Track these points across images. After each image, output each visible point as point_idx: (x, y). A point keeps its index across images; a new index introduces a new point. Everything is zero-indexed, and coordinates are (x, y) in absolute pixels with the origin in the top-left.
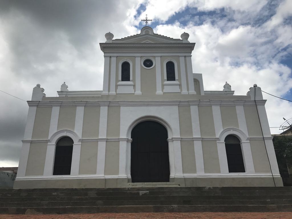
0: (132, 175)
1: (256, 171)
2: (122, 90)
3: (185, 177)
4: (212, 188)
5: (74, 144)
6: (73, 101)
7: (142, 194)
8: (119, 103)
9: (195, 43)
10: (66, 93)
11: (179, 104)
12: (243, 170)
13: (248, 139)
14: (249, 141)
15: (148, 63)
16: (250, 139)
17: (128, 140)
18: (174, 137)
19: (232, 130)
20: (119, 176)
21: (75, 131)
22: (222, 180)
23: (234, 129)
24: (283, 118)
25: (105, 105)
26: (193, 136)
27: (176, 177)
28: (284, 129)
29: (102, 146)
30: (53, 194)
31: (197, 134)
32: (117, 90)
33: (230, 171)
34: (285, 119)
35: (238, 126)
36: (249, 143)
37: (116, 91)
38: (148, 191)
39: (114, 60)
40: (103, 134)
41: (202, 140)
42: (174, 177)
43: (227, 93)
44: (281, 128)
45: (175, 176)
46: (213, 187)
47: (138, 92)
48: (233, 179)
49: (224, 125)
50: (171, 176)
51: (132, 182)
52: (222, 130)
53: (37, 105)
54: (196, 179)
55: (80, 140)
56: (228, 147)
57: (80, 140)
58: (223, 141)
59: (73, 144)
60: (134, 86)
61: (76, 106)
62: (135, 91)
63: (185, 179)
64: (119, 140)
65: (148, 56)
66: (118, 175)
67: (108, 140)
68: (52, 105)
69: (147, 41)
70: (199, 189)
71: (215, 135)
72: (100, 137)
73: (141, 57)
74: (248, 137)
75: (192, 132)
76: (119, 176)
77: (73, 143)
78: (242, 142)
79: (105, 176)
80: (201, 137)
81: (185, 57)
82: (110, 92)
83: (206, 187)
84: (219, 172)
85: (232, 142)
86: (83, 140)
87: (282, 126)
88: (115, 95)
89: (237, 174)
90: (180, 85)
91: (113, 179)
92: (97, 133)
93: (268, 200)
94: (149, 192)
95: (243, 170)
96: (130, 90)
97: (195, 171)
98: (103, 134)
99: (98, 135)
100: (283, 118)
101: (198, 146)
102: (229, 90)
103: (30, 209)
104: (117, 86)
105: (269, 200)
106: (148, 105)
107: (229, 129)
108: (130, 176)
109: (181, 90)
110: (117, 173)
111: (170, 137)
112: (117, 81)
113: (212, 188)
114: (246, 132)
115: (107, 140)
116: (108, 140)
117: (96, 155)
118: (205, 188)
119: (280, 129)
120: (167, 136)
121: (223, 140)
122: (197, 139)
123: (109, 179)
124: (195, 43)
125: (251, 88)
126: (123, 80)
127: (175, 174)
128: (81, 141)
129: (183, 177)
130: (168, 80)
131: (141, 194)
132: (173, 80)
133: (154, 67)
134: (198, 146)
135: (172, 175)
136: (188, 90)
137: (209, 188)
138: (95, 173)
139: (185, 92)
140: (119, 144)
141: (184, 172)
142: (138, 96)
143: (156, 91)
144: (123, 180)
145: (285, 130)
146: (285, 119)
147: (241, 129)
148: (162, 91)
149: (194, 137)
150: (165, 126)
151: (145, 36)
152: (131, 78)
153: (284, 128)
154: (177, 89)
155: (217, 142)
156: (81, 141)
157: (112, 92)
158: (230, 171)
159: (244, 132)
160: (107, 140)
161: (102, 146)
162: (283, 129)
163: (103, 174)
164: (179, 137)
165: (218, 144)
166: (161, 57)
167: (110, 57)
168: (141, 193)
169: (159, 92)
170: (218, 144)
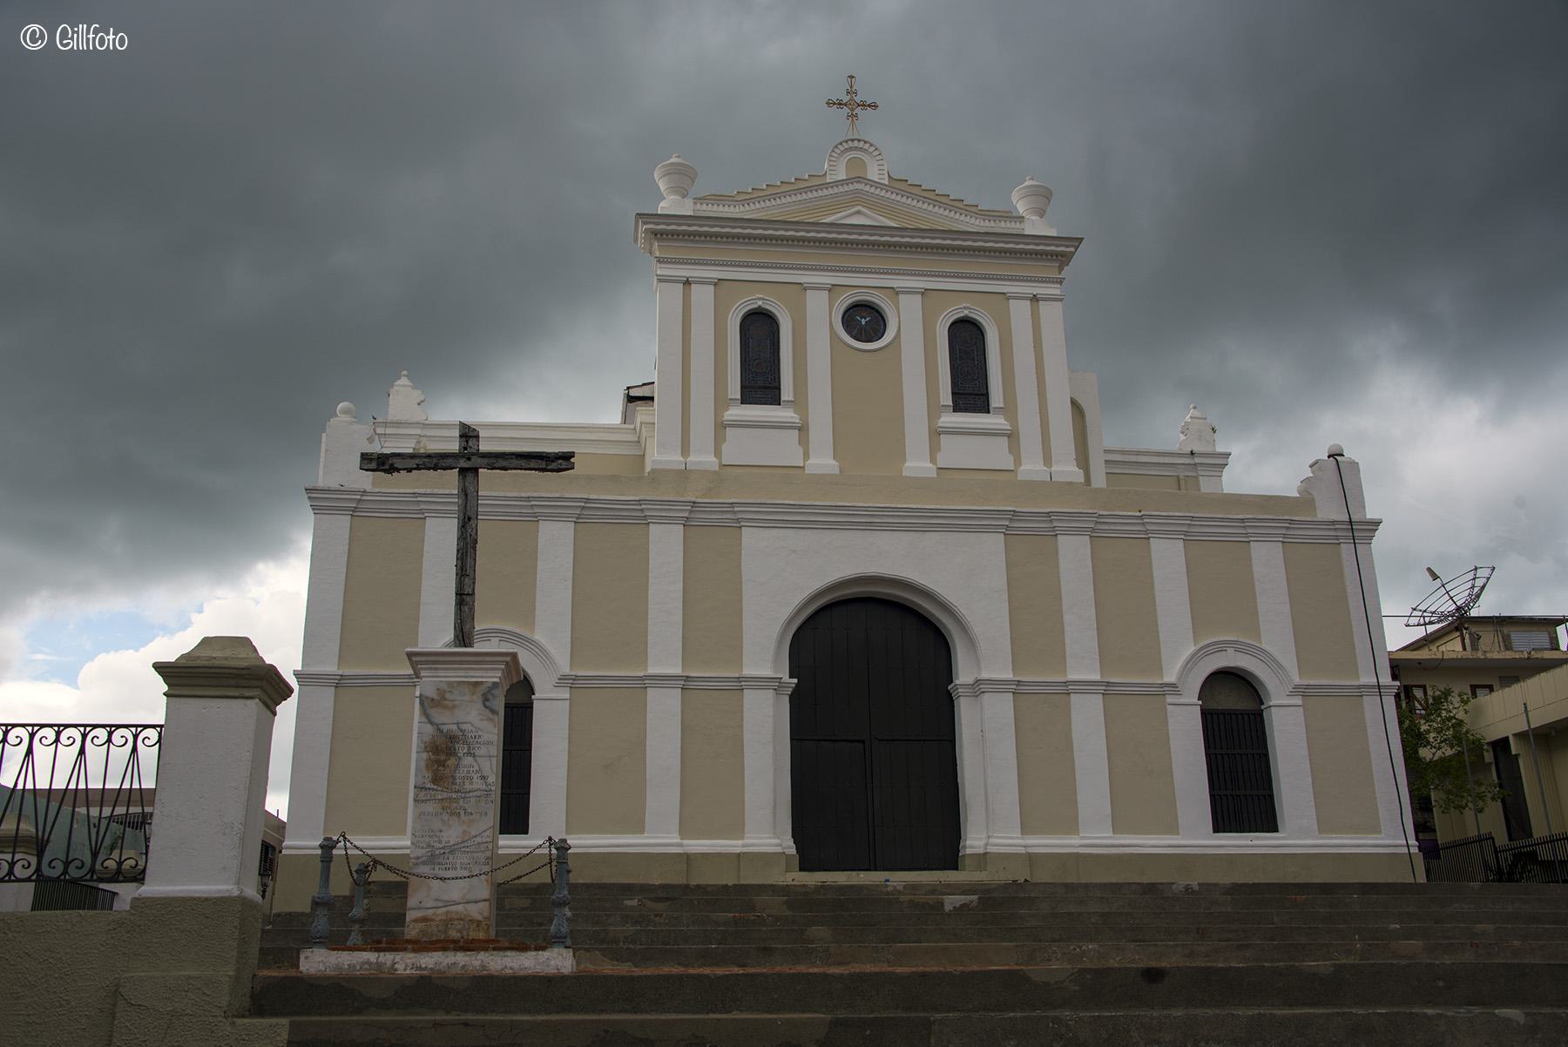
0: (797, 834)
1: (1325, 826)
2: (744, 448)
3: (1031, 850)
4: (1197, 888)
5: (537, 695)
6: (524, 495)
7: (954, 907)
8: (734, 512)
9: (1083, 239)
10: (418, 431)
11: (1011, 525)
12: (1268, 822)
13: (1301, 690)
14: (1298, 701)
15: (863, 322)
16: (1302, 691)
17: (774, 684)
18: (985, 675)
19: (1230, 651)
20: (747, 841)
21: (537, 637)
22: (1185, 861)
23: (1240, 648)
24: (1429, 570)
25: (669, 520)
26: (1065, 671)
27: (991, 849)
28: (1431, 623)
29: (664, 709)
30: (628, 903)
31: (1082, 668)
32: (724, 447)
33: (1219, 827)
34: (1435, 577)
35: (1257, 633)
36: (1301, 709)
37: (718, 453)
38: (976, 897)
39: (703, 297)
40: (665, 658)
41: (1107, 690)
42: (981, 851)
43: (1197, 460)
44: (1413, 621)
45: (986, 845)
46: (1199, 884)
47: (822, 461)
48: (1231, 860)
49: (1197, 631)
50: (972, 847)
51: (800, 870)
52: (1192, 649)
53: (355, 509)
54: (1077, 857)
55: (565, 680)
56: (1211, 720)
57: (565, 680)
58: (1195, 700)
59: (533, 697)
60: (803, 429)
61: (536, 519)
62: (806, 456)
63: (1031, 859)
64: (741, 684)
65: (864, 283)
66: (743, 838)
67: (691, 684)
68: (421, 511)
69: (858, 212)
70: (1151, 889)
71: (1159, 670)
72: (652, 671)
73: (832, 289)
74: (1297, 680)
75: (1064, 657)
76: (747, 841)
77: (534, 694)
78: (1271, 704)
79: (686, 842)
80: (1102, 677)
81: (1035, 299)
82: (692, 458)
83: (1173, 884)
84: (1173, 828)
85: (1229, 701)
86: (576, 678)
87: (1422, 607)
88: (715, 472)
89: (1246, 838)
90: (1012, 436)
91: (719, 854)
92: (638, 648)
93: (1392, 926)
94: (979, 898)
95: (1268, 822)
96: (780, 450)
97: (1070, 825)
98: (665, 658)
99: (642, 657)
100: (1429, 570)
101: (1087, 716)
102: (1209, 450)
103: (585, 949)
104: (721, 427)
105: (1398, 926)
106: (869, 526)
107: (1220, 647)
108: (789, 846)
109: (1018, 462)
110: (737, 830)
111: (964, 675)
112: (721, 403)
113: (1197, 888)
114: (1289, 661)
115: (686, 684)
116: (691, 684)
117: (638, 747)
118: (1174, 887)
119: (1411, 623)
120: (948, 674)
121: (1191, 695)
122: (1085, 686)
123: (704, 855)
124: (1083, 239)
125: (1316, 462)
126: (747, 398)
127: (989, 837)
128: (571, 682)
129: (1023, 850)
130: (957, 408)
131: (948, 908)
132: (980, 411)
133: (887, 346)
134: (1087, 716)
135: (974, 841)
136: (1048, 460)
137: (1187, 888)
138: (638, 826)
139: (1032, 467)
140: (742, 699)
141: (1026, 829)
142: (824, 481)
143: (905, 460)
144: (764, 859)
145: (1431, 629)
146: (1435, 577)
147: (1268, 648)
148: (933, 460)
149: (1072, 676)
150: (945, 626)
151: (851, 187)
152: (787, 393)
153: (1427, 620)
154: (995, 454)
155: (1170, 699)
156: (571, 682)
157: (703, 458)
158: (1219, 827)
159: (1280, 659)
160: (686, 684)
161: (664, 709)
162: (1425, 624)
163: (677, 835)
164: (1009, 675)
165: (1170, 708)
166: (924, 293)
167: (687, 283)
168: (951, 902)
169: (917, 464)
170: (1170, 708)
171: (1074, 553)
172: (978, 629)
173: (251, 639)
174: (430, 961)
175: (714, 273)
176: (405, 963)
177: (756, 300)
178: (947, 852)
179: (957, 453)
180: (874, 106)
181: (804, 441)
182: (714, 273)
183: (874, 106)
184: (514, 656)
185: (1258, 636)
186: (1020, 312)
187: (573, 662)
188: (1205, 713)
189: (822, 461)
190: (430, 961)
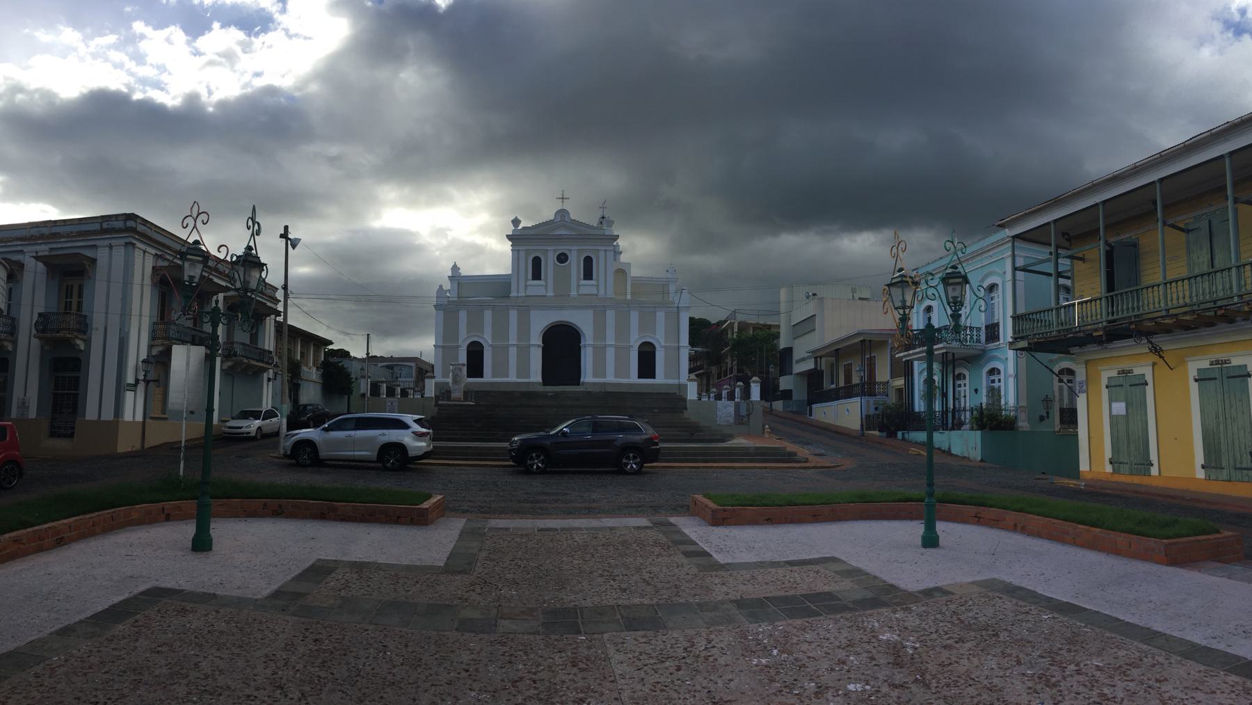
22: (631, 385)
23: (652, 338)
37: (525, 293)
47: (550, 293)
60: (546, 286)
65: (562, 248)
85: (647, 349)
126: (585, 279)
158: (640, 377)
160: (517, 346)
171: (611, 315)
172: (585, 332)
173: (708, 319)
174: (454, 403)
175: (525, 248)
176: (450, 403)
177: (538, 254)
178: (577, 382)
179: (584, 290)
180: (568, 198)
181: (546, 290)
182: (1025, 255)
183: (568, 198)
184: (142, 362)
185: (655, 334)
186: (602, 254)
187: (493, 342)
188: (639, 352)
189: (550, 293)
190: (454, 403)
